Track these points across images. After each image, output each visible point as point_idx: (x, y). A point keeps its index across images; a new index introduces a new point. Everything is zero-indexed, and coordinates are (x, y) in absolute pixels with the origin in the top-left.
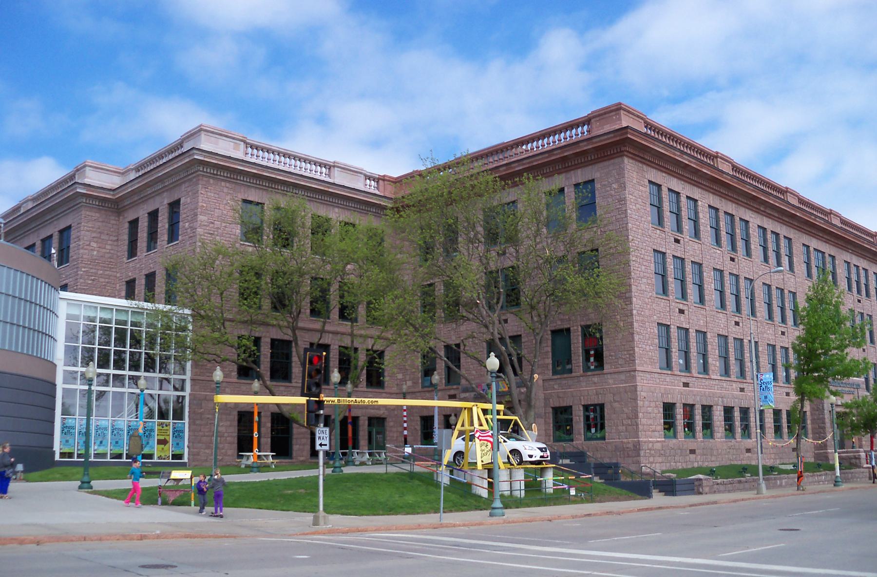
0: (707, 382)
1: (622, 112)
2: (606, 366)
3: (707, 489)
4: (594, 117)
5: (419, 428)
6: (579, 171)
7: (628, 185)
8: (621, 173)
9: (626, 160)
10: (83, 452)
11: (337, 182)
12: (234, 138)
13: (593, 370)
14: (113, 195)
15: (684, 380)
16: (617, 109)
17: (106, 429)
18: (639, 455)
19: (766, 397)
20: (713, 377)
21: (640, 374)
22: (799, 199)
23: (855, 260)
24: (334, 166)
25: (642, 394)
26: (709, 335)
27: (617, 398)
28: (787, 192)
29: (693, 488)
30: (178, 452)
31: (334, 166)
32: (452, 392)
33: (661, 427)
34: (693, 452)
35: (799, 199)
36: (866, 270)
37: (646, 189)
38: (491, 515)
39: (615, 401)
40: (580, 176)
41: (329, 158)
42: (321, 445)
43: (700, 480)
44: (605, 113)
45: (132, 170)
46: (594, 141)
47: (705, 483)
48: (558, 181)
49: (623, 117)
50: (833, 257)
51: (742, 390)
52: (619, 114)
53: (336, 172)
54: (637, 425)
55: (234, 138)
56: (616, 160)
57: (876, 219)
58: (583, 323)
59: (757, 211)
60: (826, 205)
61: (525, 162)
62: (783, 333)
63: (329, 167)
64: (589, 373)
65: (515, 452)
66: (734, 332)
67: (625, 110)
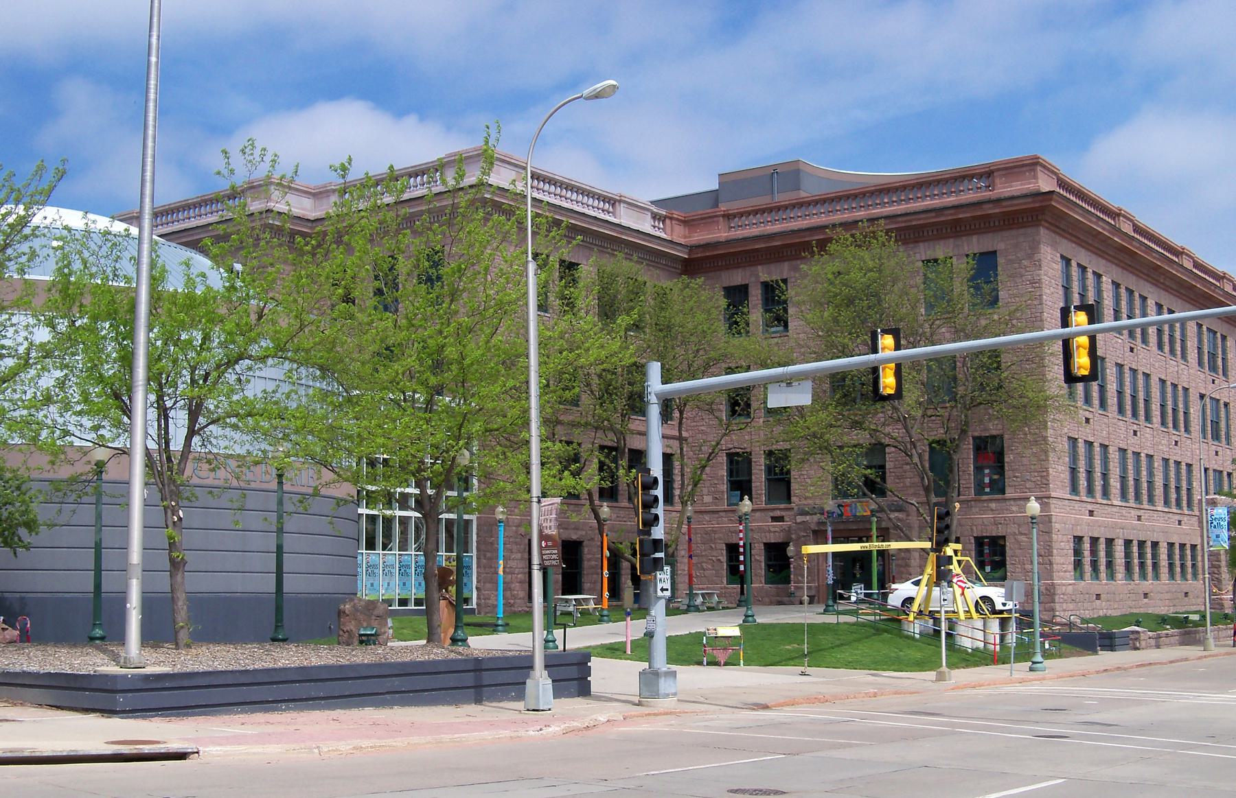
0: (1109, 509)
1: (1039, 168)
2: (1008, 490)
3: (1143, 643)
4: (998, 170)
5: (724, 559)
6: (975, 238)
7: (1044, 264)
8: (1035, 248)
9: (1042, 231)
10: (422, 595)
11: (625, 222)
12: (516, 166)
13: (987, 494)
14: (311, 228)
15: (1090, 507)
16: (1032, 165)
17: (393, 566)
18: (1053, 602)
19: (1218, 536)
20: (1115, 503)
21: (1054, 501)
22: (1134, 225)
23: (1081, 256)
24: (620, 201)
25: (1056, 526)
26: (1111, 449)
27: (1022, 530)
28: (1182, 253)
29: (1132, 643)
30: (1028, 608)
31: (620, 201)
32: (778, 513)
33: (1071, 567)
34: (1098, 596)
35: (1134, 225)
36: (1098, 276)
37: (1058, 266)
38: (1031, 670)
39: (1021, 534)
40: (977, 244)
41: (612, 189)
42: (662, 590)
43: (1138, 632)
44: (1015, 167)
45: (334, 191)
46: (1004, 203)
47: (1142, 636)
48: (940, 250)
49: (1040, 175)
50: (1083, 269)
51: (1139, 518)
52: (1034, 170)
53: (622, 208)
54: (1051, 564)
55: (516, 166)
56: (1029, 230)
57: (1235, 258)
58: (976, 434)
59: (1156, 284)
60: (1177, 241)
61: (900, 219)
62: (1135, 433)
63: (613, 202)
64: (985, 497)
65: (985, 599)
66: (1132, 445)
67: (1125, 217)
